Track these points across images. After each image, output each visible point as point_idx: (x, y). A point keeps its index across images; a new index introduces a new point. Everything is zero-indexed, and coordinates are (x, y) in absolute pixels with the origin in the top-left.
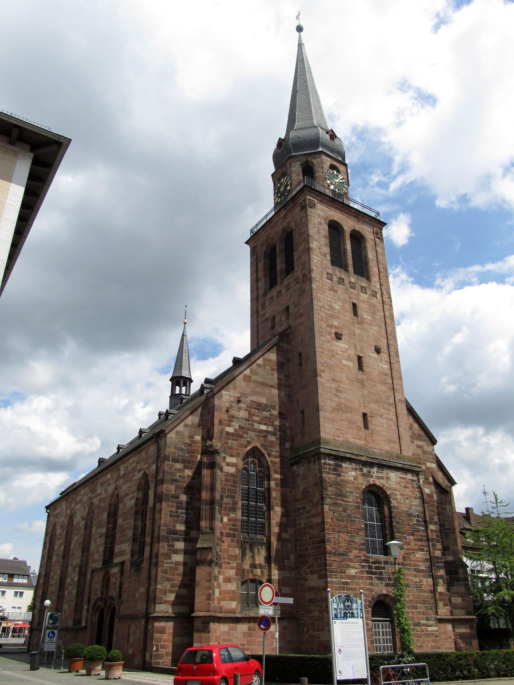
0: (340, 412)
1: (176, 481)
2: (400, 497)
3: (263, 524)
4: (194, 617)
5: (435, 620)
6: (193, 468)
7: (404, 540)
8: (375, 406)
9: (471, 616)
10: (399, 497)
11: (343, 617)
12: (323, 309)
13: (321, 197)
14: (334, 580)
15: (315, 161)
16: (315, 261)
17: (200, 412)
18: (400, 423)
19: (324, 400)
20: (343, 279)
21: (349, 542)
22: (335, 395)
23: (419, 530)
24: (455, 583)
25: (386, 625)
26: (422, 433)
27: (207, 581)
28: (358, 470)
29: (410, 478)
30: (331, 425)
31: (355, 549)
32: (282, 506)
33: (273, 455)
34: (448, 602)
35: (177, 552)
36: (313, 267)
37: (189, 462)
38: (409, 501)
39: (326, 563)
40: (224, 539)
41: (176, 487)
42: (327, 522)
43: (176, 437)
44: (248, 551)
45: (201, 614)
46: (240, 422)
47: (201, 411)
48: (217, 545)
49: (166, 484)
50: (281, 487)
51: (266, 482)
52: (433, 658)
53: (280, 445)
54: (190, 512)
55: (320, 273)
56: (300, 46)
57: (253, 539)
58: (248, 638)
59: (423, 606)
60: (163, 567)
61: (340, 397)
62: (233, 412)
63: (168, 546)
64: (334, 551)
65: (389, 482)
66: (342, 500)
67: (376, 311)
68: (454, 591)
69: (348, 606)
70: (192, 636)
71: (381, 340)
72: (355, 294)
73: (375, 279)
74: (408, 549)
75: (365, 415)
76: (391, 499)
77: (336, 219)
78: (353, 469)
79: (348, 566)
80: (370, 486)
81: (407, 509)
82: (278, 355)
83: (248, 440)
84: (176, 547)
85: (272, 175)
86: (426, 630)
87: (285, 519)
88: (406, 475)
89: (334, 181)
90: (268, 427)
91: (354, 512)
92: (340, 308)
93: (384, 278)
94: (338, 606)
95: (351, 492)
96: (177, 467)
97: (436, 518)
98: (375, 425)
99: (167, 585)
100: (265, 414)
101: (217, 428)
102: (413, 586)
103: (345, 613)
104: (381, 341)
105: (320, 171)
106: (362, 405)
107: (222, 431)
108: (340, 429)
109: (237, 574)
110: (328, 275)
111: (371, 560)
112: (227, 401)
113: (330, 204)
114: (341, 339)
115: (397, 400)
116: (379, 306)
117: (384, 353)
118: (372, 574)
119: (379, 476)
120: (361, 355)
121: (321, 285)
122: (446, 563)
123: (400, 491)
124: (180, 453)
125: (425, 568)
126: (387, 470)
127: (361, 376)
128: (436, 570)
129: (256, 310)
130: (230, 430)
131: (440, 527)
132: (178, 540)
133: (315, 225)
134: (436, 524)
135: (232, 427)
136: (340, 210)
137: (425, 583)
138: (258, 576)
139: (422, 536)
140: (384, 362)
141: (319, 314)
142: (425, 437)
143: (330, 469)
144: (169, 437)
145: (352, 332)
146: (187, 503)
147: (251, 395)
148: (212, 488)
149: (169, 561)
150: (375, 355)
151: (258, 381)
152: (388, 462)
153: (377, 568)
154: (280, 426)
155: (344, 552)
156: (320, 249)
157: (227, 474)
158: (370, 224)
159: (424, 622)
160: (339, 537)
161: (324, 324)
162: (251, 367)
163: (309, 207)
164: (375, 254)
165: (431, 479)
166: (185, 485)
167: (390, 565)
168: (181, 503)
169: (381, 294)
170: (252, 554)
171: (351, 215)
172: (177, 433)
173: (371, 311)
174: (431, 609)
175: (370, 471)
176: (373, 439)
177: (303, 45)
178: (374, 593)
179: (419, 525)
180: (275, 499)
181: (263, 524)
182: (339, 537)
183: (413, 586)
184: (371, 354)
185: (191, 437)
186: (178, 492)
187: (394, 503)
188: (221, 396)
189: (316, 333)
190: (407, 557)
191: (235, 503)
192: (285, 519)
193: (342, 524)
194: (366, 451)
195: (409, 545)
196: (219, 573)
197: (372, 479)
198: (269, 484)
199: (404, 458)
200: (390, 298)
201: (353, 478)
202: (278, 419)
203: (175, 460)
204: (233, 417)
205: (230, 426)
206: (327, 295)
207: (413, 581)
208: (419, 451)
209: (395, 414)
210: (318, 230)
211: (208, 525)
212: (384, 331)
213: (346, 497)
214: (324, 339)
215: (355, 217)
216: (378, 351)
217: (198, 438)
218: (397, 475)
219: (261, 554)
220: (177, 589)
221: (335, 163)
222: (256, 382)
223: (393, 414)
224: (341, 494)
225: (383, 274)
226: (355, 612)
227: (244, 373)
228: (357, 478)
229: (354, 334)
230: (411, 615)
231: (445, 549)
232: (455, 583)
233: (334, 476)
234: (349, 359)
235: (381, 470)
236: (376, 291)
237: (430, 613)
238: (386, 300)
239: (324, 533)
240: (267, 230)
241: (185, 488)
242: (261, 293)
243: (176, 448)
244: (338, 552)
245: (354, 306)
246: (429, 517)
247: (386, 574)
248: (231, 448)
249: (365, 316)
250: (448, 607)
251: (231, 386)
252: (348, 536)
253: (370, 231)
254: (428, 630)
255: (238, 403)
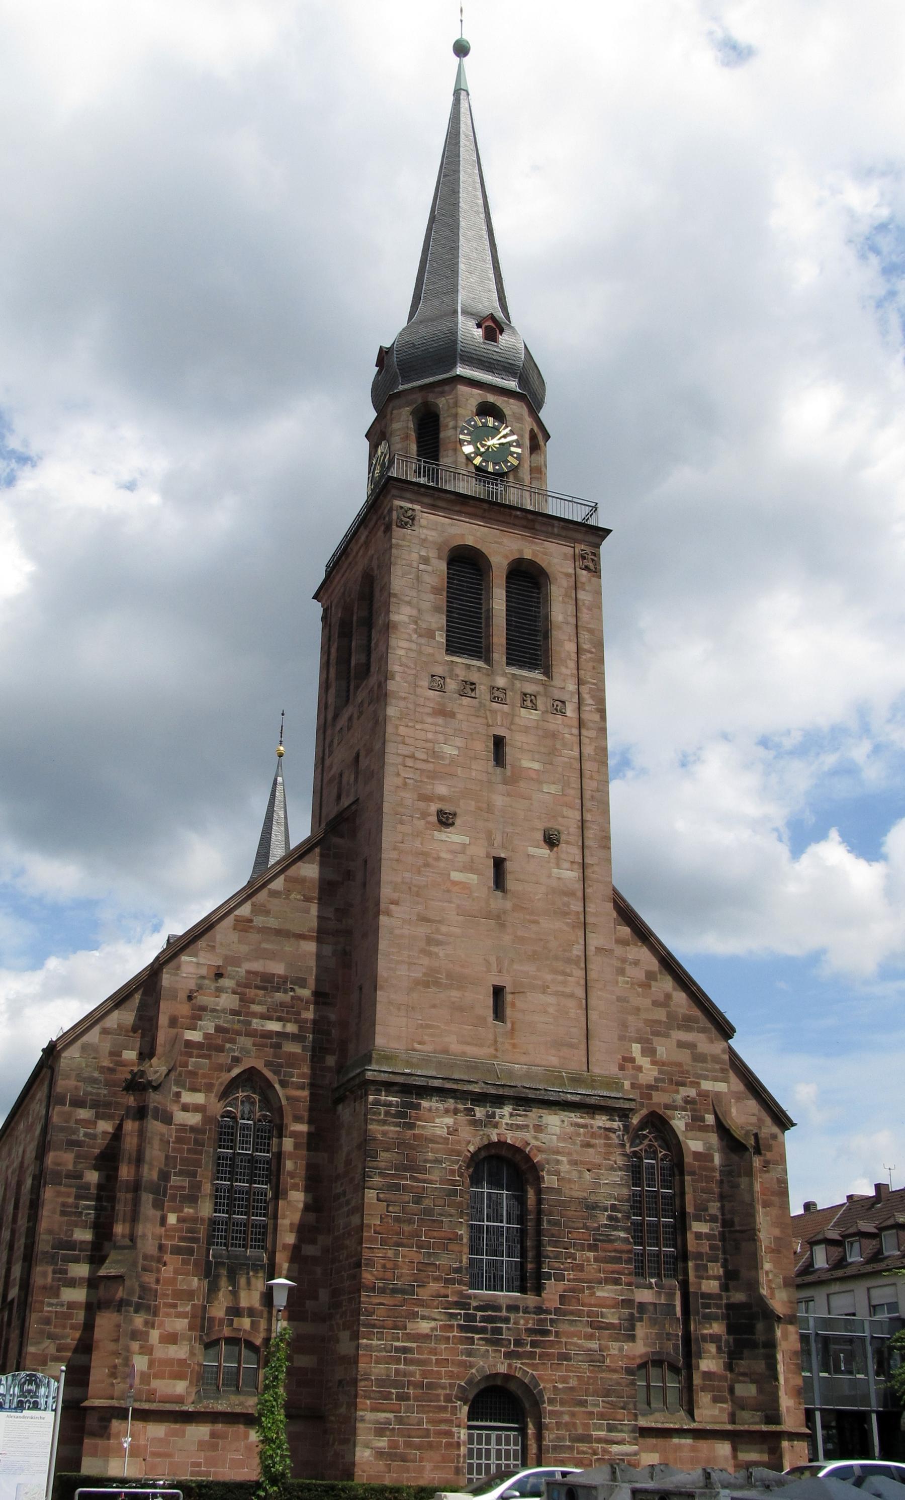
0: (433, 989)
1: (78, 1144)
2: (568, 1167)
3: (265, 1227)
4: (86, 1408)
5: (633, 1431)
6: (116, 1118)
7: (569, 1261)
8: (529, 968)
9: (774, 1426)
10: (565, 1167)
11: (15, 1408)
12: (409, 762)
13: (432, 496)
14: (375, 1342)
15: (442, 402)
16: (401, 652)
17: (137, 1001)
18: (593, 1002)
19: (393, 966)
20: (472, 684)
21: (421, 1265)
22: (423, 951)
23: (612, 1238)
24: (746, 1352)
25: (507, 1437)
26: (697, 1013)
27: (112, 1341)
28: (461, 1112)
29: (601, 1125)
30: (405, 1019)
31: (436, 1279)
32: (307, 1190)
33: (293, 1083)
34: (726, 1394)
35: (72, 1283)
36: (395, 667)
37: (108, 1105)
38: (593, 1175)
39: (359, 1309)
40: (167, 1257)
41: (78, 1156)
42: (369, 1226)
43: (81, 1057)
44: (223, 1282)
45: (97, 1403)
46: (219, 1018)
47: (141, 1000)
48: (145, 1269)
49: (55, 1150)
50: (309, 1150)
51: (275, 1140)
52: (317, 1490)
53: (312, 1061)
54: (105, 1204)
55: (411, 678)
56: (459, 92)
57: (236, 1257)
58: (208, 1454)
59: (603, 1401)
60: (42, 1312)
61: (437, 954)
62: (203, 999)
63: (54, 1272)
64: (380, 1284)
65: (541, 1135)
66: (412, 1177)
67: (558, 746)
68: (742, 1370)
69: (29, 1391)
70: (81, 1443)
71: (565, 813)
72: (503, 713)
73: (564, 670)
74: (574, 1280)
75: (498, 992)
76: (544, 1174)
77: (470, 541)
78: (447, 1111)
79: (415, 1315)
80: (490, 1145)
81: (585, 1195)
82: (322, 865)
83: (236, 1054)
84: (71, 1274)
85: (366, 436)
86: (605, 1451)
87: (312, 1217)
88: (593, 1118)
89: (483, 446)
90: (284, 1026)
91: (440, 1202)
92: (456, 752)
93: (591, 664)
94: (8, 1390)
95: (437, 1161)
96: (82, 1117)
97: (714, 1208)
98: (523, 1011)
99: (50, 1347)
100: (279, 996)
101: (163, 1035)
102: (580, 1358)
103: (20, 1402)
104: (564, 817)
105: (451, 424)
106: (494, 967)
107: (175, 1039)
108: (428, 1026)
109: (191, 1328)
110: (433, 681)
111: (474, 1304)
112: (190, 976)
113: (457, 508)
114: (453, 824)
115: (591, 949)
116: (569, 735)
117: (568, 843)
118: (472, 1333)
119: (517, 1125)
120: (503, 856)
121: (411, 706)
122: (730, 1306)
123: (569, 1154)
124: (89, 1089)
125: (620, 1319)
126: (540, 1111)
127: (498, 902)
128: (700, 1323)
129: (321, 755)
130: (194, 1036)
131: (723, 1226)
132: (76, 1260)
133: (410, 566)
134: (713, 1219)
135: (200, 1030)
136: (482, 518)
137: (613, 1352)
138: (245, 1331)
139: (621, 1252)
140: (566, 865)
141: (398, 775)
142: (704, 1022)
143: (387, 1113)
144: (65, 1058)
145: (485, 806)
146: (100, 1187)
147: (249, 960)
148: (139, 1160)
149: (54, 1301)
150: (545, 852)
151: (270, 928)
152: (542, 1092)
153: (484, 1319)
154: (315, 1022)
155: (406, 1287)
156: (416, 623)
157: (183, 1128)
158: (565, 538)
159: (602, 1434)
160: (397, 1254)
161: (409, 797)
162: (254, 899)
163: (398, 526)
164: (571, 609)
165: (710, 1119)
166: (97, 1151)
167: (524, 1313)
168: (87, 1186)
169: (577, 705)
170: (234, 1287)
171: (514, 525)
172: (84, 1048)
173: (543, 750)
174: (623, 1408)
175: (494, 1113)
176: (515, 1041)
177: (467, 91)
178: (474, 1371)
179: (616, 1228)
180: (292, 1175)
181: (265, 1227)
182: (397, 1254)
183: (580, 1358)
184: (532, 850)
185: (115, 1054)
186: (80, 1166)
187: (549, 1181)
188: (178, 968)
189: (386, 818)
190: (573, 1297)
191: (196, 1187)
192: (312, 1217)
193: (406, 1228)
194: (491, 1070)
195: (582, 1270)
196: (150, 1324)
197: (496, 1131)
198: (280, 1145)
199: (594, 1081)
200: (602, 712)
201: (446, 1130)
202: (312, 1007)
203: (78, 1103)
204: (203, 1008)
205: (195, 1029)
206: (426, 726)
207: (583, 1347)
208: (684, 1056)
209: (583, 982)
210: (418, 578)
211: (127, 1232)
212: (574, 793)
213: (425, 1170)
214: (406, 829)
215: (525, 527)
216: (551, 841)
217: (130, 1055)
218: (566, 1119)
219: (253, 1287)
220: (69, 1354)
221: (491, 398)
222: (264, 930)
223: (578, 983)
224: (411, 1166)
225: (589, 655)
226: (42, 1401)
227: (237, 913)
228: (456, 1130)
229: (490, 809)
230: (566, 1418)
231: (730, 1278)
232: (746, 1352)
233: (398, 1129)
234: (470, 867)
235: (524, 1110)
236: (563, 699)
237: (620, 1417)
238: (590, 716)
239: (362, 1248)
240: (342, 571)
241: (96, 1158)
242: (330, 716)
243: (79, 1078)
244: (391, 1286)
245: (499, 743)
246: (695, 1206)
247: (510, 1333)
248: (193, 1074)
249: (526, 763)
250: (725, 1406)
251: (202, 943)
252: (421, 1252)
253: (565, 554)
254: (610, 1452)
255: (216, 980)
